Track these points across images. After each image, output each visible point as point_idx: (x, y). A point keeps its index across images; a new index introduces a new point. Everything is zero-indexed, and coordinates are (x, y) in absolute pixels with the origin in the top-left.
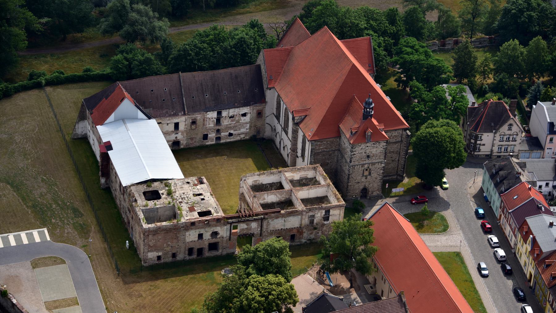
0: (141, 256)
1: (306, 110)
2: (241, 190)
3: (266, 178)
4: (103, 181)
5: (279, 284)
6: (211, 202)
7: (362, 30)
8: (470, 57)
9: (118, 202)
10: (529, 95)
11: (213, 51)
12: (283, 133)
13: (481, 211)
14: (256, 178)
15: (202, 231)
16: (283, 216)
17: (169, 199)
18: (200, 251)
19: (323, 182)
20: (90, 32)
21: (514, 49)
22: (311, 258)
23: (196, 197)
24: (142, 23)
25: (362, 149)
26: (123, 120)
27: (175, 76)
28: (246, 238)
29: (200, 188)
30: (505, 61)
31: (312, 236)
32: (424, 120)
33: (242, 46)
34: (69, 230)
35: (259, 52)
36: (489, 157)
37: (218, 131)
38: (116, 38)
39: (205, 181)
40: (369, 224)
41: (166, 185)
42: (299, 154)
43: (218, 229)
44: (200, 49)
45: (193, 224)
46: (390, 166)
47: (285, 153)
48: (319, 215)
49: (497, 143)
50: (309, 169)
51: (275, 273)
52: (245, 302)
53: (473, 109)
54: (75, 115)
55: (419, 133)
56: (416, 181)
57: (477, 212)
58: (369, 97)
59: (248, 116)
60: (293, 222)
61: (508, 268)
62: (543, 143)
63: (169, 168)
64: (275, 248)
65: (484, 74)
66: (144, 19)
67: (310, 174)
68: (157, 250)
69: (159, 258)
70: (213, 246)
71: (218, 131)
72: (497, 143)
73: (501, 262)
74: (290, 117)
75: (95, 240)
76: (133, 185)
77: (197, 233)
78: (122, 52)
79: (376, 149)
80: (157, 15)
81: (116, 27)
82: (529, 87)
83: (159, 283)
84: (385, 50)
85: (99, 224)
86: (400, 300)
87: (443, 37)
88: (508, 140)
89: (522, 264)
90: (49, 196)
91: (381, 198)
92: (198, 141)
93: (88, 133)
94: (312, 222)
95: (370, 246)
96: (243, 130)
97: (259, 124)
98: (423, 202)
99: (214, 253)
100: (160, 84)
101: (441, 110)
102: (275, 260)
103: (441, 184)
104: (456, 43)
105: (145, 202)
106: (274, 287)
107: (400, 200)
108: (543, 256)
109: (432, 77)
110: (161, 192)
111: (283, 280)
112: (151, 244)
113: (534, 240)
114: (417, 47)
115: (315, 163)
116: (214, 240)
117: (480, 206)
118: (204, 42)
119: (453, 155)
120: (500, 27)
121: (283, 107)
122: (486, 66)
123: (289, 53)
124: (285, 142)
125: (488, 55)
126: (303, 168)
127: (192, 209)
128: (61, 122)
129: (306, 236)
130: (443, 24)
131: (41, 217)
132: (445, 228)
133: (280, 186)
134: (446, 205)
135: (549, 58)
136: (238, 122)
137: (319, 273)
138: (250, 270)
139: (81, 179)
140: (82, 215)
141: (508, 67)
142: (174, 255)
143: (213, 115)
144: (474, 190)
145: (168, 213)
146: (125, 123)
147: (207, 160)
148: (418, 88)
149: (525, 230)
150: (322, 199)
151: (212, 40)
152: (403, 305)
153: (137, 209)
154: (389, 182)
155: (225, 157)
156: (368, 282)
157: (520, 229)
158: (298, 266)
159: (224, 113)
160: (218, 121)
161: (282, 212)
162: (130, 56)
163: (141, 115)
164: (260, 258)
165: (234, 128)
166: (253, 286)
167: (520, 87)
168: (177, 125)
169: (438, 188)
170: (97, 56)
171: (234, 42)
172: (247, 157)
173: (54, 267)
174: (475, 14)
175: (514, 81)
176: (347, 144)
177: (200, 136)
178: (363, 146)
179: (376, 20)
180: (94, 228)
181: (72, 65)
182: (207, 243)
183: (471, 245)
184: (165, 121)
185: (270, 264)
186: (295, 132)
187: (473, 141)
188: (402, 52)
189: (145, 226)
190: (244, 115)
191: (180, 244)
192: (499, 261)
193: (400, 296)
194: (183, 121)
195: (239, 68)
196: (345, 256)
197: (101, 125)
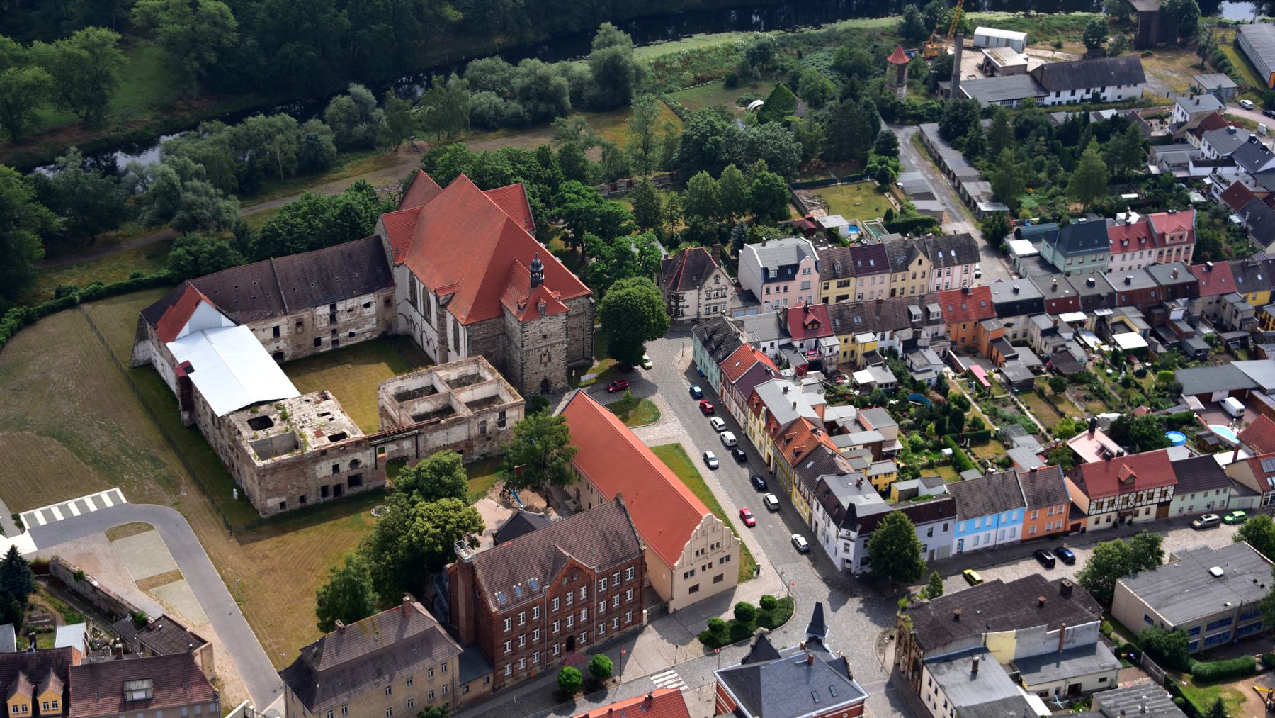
0: (258, 506)
1: (454, 286)
2: (381, 403)
3: (412, 382)
4: (185, 416)
5: (457, 509)
6: (343, 422)
7: (508, 177)
8: (652, 199)
9: (212, 441)
10: (731, 240)
11: (310, 226)
12: (425, 323)
13: (697, 389)
14: (399, 383)
15: (337, 461)
16: (444, 427)
17: (285, 425)
18: (338, 489)
19: (489, 377)
20: (128, 228)
21: (704, 183)
22: (488, 477)
23: (323, 419)
24: (202, 206)
25: (537, 327)
26: (202, 330)
27: (266, 263)
28: (397, 463)
29: (325, 406)
30: (695, 200)
31: (486, 450)
32: (609, 283)
33: (349, 214)
34: (150, 485)
35: (374, 223)
36: (696, 321)
37: (334, 332)
38: (167, 231)
39: (330, 395)
40: (561, 420)
41: (278, 408)
42: (451, 346)
43: (358, 456)
44: (292, 225)
45: (324, 453)
46: (573, 348)
47: (431, 349)
48: (492, 420)
49: (703, 302)
50: (468, 363)
51: (450, 497)
52: (415, 538)
53: (667, 263)
54: (130, 336)
55: (605, 298)
56: (611, 362)
57: (692, 392)
58: (536, 257)
59: (373, 307)
60: (459, 434)
61: (741, 453)
62: (758, 296)
63: (278, 385)
64: (445, 464)
65: (672, 219)
66: (204, 199)
67: (471, 370)
68: (279, 495)
69: (283, 505)
70: (354, 480)
71: (334, 332)
72: (703, 302)
73: (731, 447)
74: (433, 299)
75: (189, 493)
76: (232, 413)
77: (331, 465)
78: (181, 245)
79: (554, 325)
80: (220, 192)
81: (165, 216)
82: (730, 229)
83: (288, 537)
84: (542, 201)
85: (191, 472)
86: (619, 504)
87: (612, 179)
88: (716, 297)
89: (757, 445)
90: (114, 446)
91: (568, 390)
92: (308, 349)
93: (153, 358)
94: (483, 431)
95: (567, 446)
96: (368, 327)
97: (389, 315)
98: (624, 388)
99: (357, 489)
100: (246, 275)
101: (628, 266)
102: (445, 479)
103: (642, 362)
104: (630, 184)
105: (252, 433)
106: (451, 513)
107: (593, 389)
108: (782, 430)
109: (609, 227)
110: (272, 417)
111: (460, 503)
112: (270, 487)
113: (768, 412)
114: (583, 191)
115: (475, 354)
116: (355, 472)
117: (694, 384)
118: (297, 216)
119: (653, 321)
120: (682, 159)
121: (420, 287)
122: (673, 208)
123: (417, 215)
124: (428, 334)
125: (674, 194)
126: (461, 363)
127: (319, 434)
128: (112, 348)
129: (478, 450)
130: (609, 162)
131: (108, 474)
132: (655, 417)
133: (432, 390)
134: (653, 389)
135: (748, 190)
136: (360, 315)
137: (502, 494)
138: (415, 497)
139: (154, 418)
140: (165, 465)
141: (701, 207)
142: (303, 499)
143: (324, 310)
144: (684, 365)
145: (287, 444)
146: (205, 335)
147: (326, 372)
148: (595, 242)
149: (756, 401)
150: (493, 399)
151: (306, 213)
152: (623, 510)
153: (244, 443)
154: (576, 369)
155: (350, 366)
156: (568, 497)
157: (750, 402)
158: (858, 199)
159: (340, 306)
160: (333, 317)
161: (443, 422)
162: (194, 248)
163: (225, 321)
164: (426, 479)
165: (356, 325)
166: (422, 516)
167: (719, 231)
168: (276, 331)
169: (639, 368)
170: (143, 258)
171: (338, 211)
172: (379, 362)
173: (139, 535)
174: (647, 147)
175: (711, 224)
176: (515, 324)
177: (310, 341)
178: (536, 323)
179: (525, 163)
180: (184, 479)
181: (112, 272)
182: (345, 477)
183: (691, 433)
184: (261, 325)
185: (438, 485)
186: (442, 318)
187: (673, 303)
188: (564, 200)
189: (259, 463)
190: (367, 305)
191: (310, 482)
192: (728, 448)
193: (617, 499)
194: (284, 323)
195: (352, 243)
196: (537, 466)
197: (173, 340)
